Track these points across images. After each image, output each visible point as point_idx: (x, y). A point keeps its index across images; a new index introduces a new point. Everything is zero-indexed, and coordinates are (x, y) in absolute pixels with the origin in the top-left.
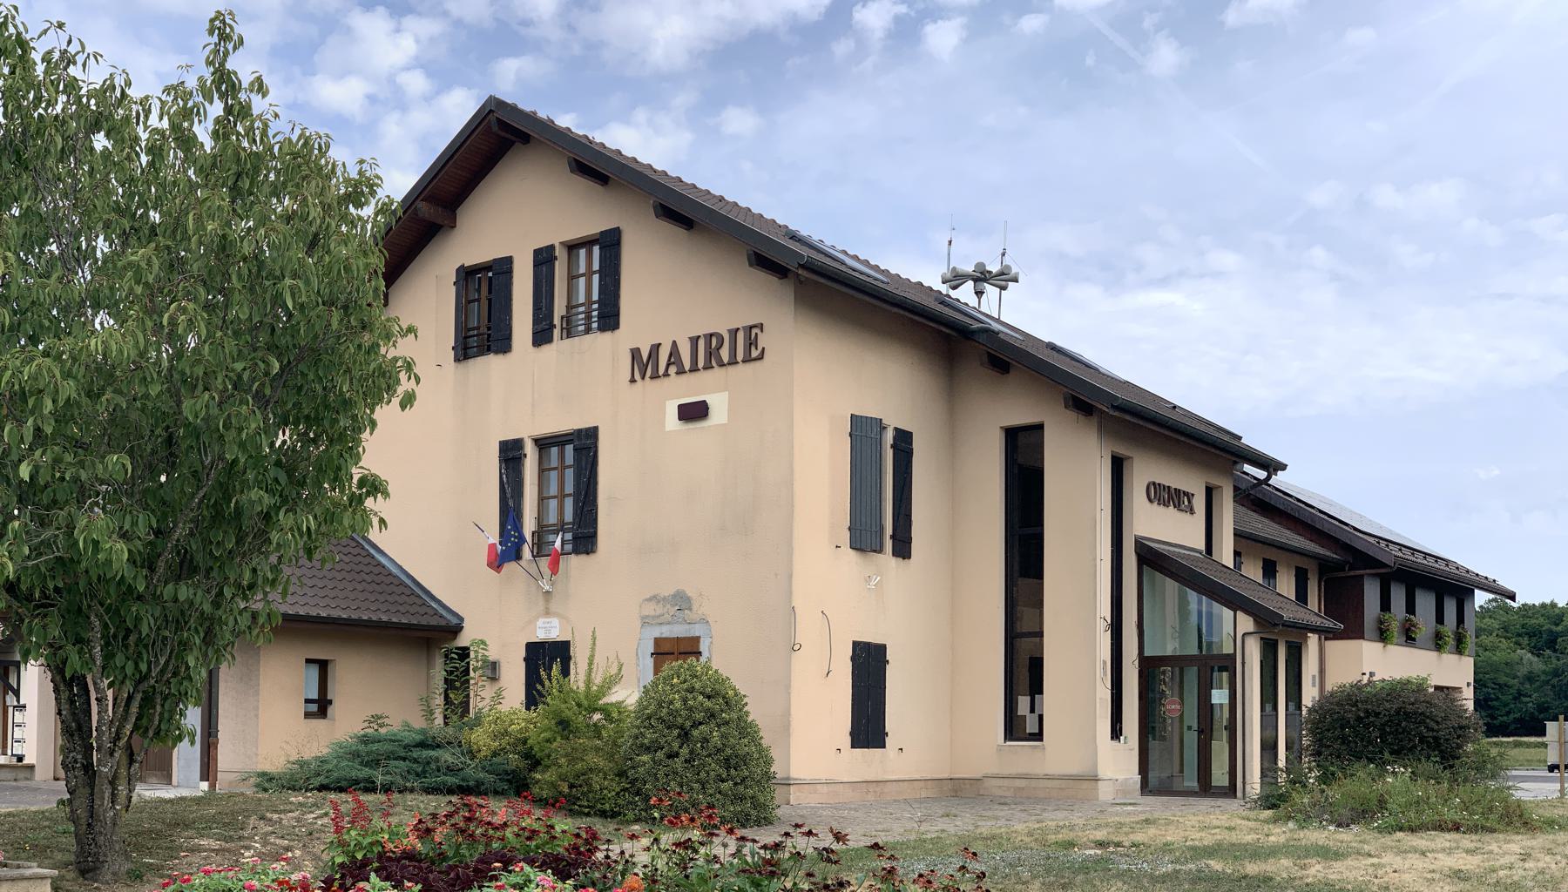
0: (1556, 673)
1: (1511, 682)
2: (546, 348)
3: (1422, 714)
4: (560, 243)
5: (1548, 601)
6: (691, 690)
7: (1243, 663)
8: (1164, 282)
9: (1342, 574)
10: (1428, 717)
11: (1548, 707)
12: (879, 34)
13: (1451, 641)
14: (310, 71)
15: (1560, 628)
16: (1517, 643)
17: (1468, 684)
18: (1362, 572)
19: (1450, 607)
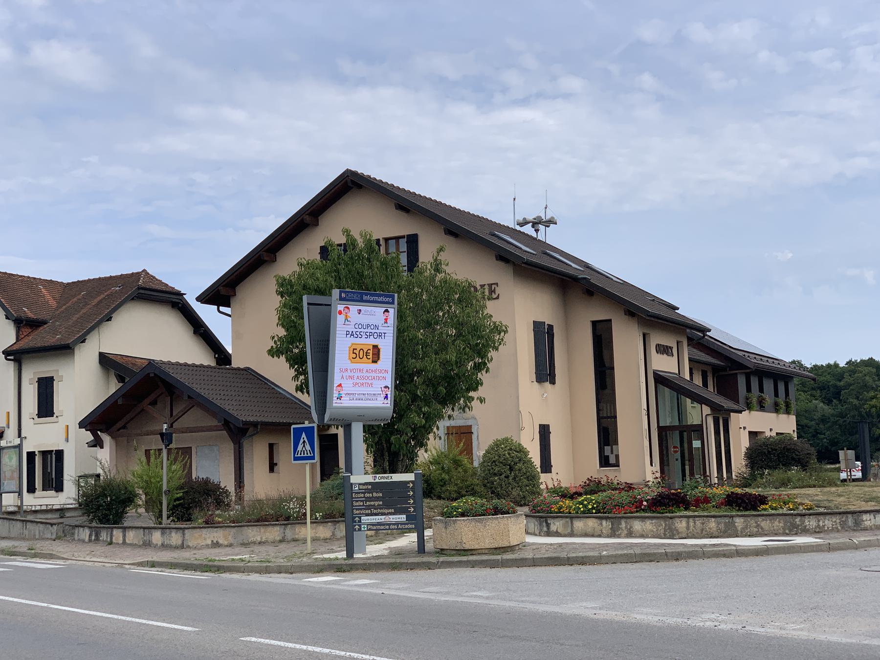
0: (842, 415)
3: (793, 449)
4: (383, 238)
5: (832, 363)
6: (511, 449)
7: (707, 428)
8: (524, 102)
10: (796, 450)
11: (837, 442)
13: (783, 407)
15: (842, 383)
17: (794, 431)
18: (737, 371)
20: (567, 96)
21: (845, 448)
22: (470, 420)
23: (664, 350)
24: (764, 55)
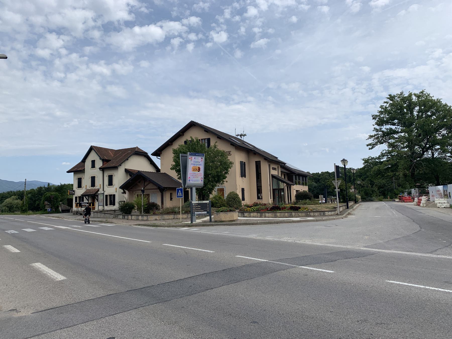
1: (312, 188)
5: (317, 172)
6: (234, 194)
8: (238, 103)
9: (290, 175)
12: (177, 46)
13: (305, 184)
14: (36, 47)
15: (320, 178)
16: (312, 181)
19: (304, 179)
20: (249, 102)
23: (274, 169)
24: (301, 92)
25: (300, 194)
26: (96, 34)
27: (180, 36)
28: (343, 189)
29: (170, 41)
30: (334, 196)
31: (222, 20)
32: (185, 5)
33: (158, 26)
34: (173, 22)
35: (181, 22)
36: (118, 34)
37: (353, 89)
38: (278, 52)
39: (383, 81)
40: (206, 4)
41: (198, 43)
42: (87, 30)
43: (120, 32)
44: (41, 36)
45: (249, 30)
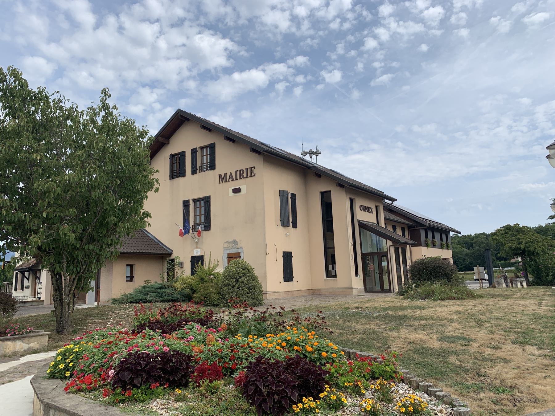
0: (473, 253)
2: (195, 175)
5: (469, 234)
6: (238, 268)
7: (390, 254)
8: (359, 152)
12: (282, 91)
13: (445, 246)
15: (473, 241)
17: (451, 257)
20: (373, 150)
21: (478, 266)
22: (239, 249)
23: (364, 209)
24: (439, 135)
25: (422, 264)
26: (192, 84)
27: (286, 79)
28: (536, 250)
29: (274, 87)
30: (496, 266)
31: (334, 57)
32: (291, 44)
33: (259, 70)
34: (277, 64)
35: (287, 64)
36: (215, 82)
37: (510, 128)
38: (406, 88)
39: (550, 115)
40: (314, 41)
41: (307, 86)
42: (182, 81)
43: (218, 80)
44: (134, 92)
45: (368, 66)
